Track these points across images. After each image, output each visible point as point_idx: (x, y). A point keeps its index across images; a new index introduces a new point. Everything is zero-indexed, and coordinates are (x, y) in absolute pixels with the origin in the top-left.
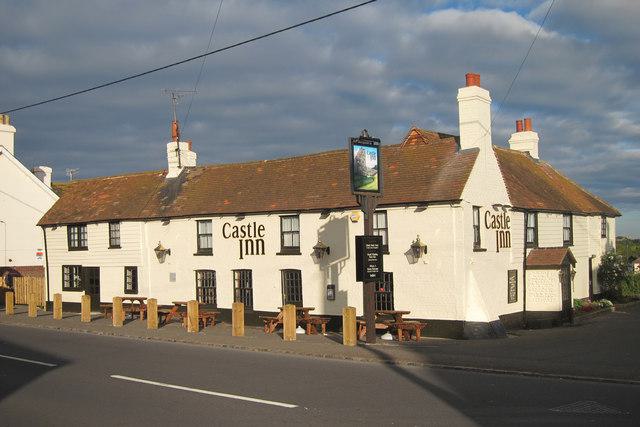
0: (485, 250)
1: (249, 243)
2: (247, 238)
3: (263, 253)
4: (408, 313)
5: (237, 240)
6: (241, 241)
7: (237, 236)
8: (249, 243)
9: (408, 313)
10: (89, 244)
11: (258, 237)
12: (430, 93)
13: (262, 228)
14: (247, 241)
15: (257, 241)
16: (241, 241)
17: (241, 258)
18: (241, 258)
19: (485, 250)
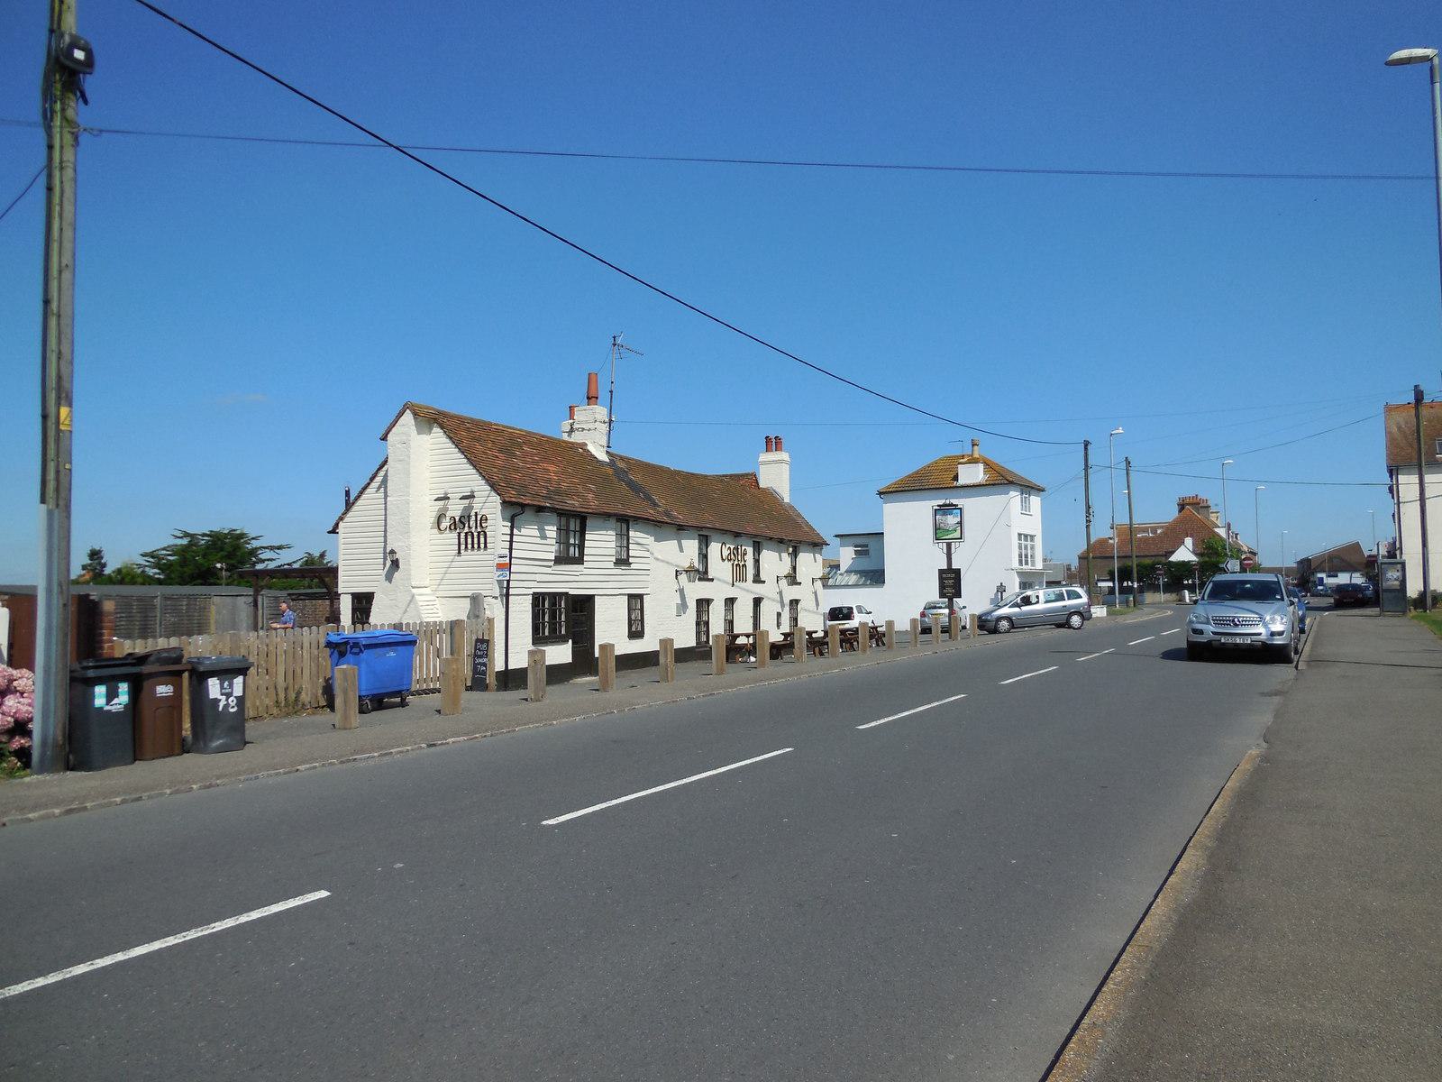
2: (466, 530)
3: (486, 546)
6: (459, 533)
9: (816, 632)
11: (479, 530)
15: (479, 533)
16: (459, 533)
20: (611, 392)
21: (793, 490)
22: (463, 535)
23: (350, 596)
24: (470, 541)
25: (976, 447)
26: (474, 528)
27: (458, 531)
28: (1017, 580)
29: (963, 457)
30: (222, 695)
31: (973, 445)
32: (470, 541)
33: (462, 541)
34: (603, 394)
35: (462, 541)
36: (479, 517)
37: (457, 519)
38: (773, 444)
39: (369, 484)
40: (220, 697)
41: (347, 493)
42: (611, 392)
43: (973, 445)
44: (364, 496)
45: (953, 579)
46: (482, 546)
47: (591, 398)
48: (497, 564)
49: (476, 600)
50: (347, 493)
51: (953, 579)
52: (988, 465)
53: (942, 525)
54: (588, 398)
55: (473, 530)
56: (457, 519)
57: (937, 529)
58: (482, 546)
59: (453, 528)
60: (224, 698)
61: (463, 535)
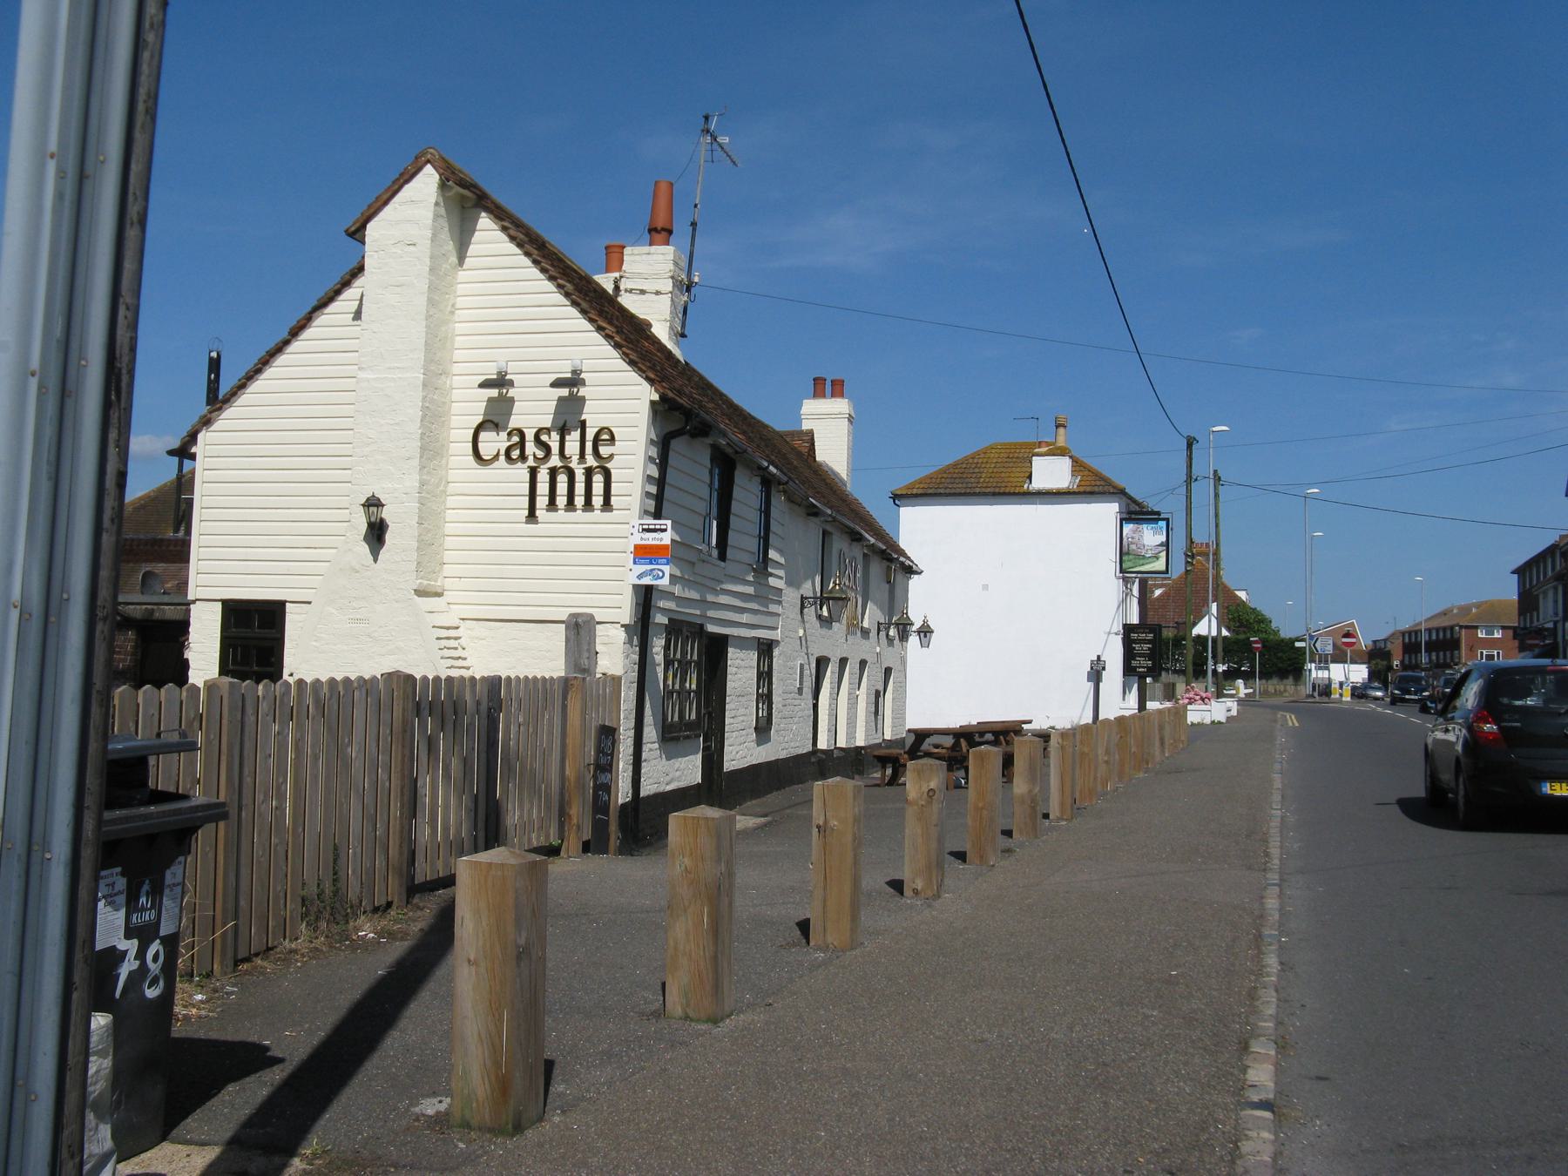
0: (1124, 699)
1: (562, 480)
2: (555, 461)
3: (607, 505)
4: (1030, 722)
5: (521, 472)
6: (533, 472)
7: (523, 457)
8: (562, 480)
9: (1030, 722)
10: (552, 522)
11: (591, 461)
12: (1047, 1110)
13: (1246, 688)
14: (553, 473)
15: (589, 473)
16: (533, 472)
17: (532, 516)
18: (532, 516)
19: (1124, 699)
20: (694, 224)
21: (854, 466)
22: (543, 476)
23: (220, 604)
24: (562, 487)
25: (1061, 430)
26: (575, 458)
27: (531, 462)
28: (871, 635)
29: (1040, 444)
30: (128, 936)
31: (1057, 427)
32: (562, 487)
33: (543, 487)
34: (681, 229)
35: (543, 487)
36: (590, 434)
37: (530, 435)
38: (820, 388)
39: (287, 343)
40: (123, 945)
41: (215, 365)
42: (694, 224)
43: (1057, 427)
44: (270, 372)
45: (1149, 642)
46: (597, 501)
47: (659, 233)
48: (636, 547)
49: (580, 630)
50: (215, 365)
51: (1149, 642)
52: (1078, 466)
53: (1133, 547)
54: (650, 231)
55: (574, 464)
56: (530, 435)
57: (1123, 553)
58: (597, 501)
59: (515, 454)
60: (131, 946)
61: (543, 476)
